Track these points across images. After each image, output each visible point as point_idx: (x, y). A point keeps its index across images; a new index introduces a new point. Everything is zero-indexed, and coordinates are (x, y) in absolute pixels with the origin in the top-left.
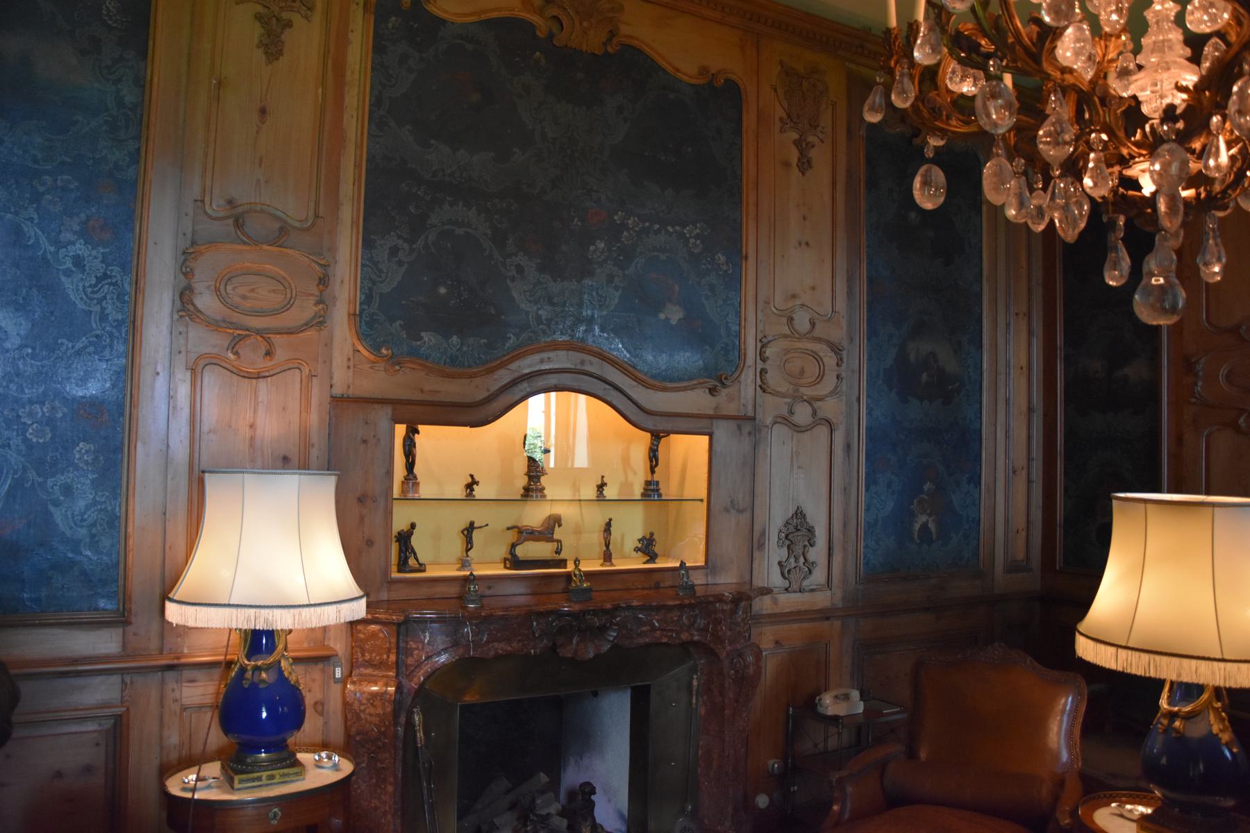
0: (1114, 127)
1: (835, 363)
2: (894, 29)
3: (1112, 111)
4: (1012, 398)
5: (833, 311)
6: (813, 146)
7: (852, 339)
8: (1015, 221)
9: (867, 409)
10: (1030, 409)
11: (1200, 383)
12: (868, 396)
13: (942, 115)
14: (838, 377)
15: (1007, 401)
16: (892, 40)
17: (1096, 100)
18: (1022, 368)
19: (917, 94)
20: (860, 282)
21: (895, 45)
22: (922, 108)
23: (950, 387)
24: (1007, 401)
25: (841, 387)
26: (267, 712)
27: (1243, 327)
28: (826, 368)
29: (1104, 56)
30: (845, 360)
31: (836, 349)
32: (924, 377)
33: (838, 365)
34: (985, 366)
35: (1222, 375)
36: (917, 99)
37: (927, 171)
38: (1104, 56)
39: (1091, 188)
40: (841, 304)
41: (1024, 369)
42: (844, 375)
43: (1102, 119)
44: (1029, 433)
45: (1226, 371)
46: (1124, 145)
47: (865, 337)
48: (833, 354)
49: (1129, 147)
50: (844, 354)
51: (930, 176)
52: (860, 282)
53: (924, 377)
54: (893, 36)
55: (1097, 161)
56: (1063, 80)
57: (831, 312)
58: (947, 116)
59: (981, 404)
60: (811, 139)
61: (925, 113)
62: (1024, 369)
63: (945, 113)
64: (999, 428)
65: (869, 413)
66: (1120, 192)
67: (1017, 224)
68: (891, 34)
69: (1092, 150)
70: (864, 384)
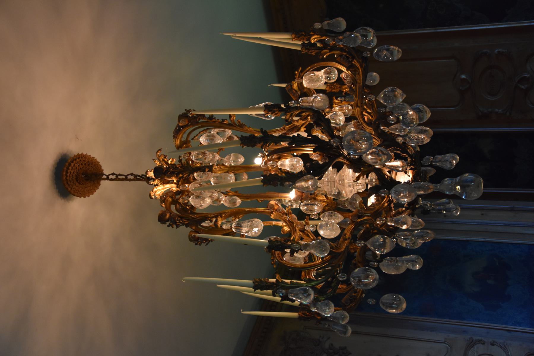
0: (373, 211)
1: (482, 345)
2: (299, 315)
3: (366, 212)
4: (504, 222)
5: (444, 343)
6: (332, 345)
7: (464, 331)
8: (422, 265)
9: (516, 326)
10: (512, 210)
11: (497, 110)
12: (506, 324)
13: (355, 296)
14: (493, 345)
15: (506, 225)
16: (306, 316)
17: (359, 220)
18: (482, 214)
19: (341, 308)
20: (423, 321)
21: (309, 315)
22: (349, 307)
23: (497, 264)
24: (506, 225)
25: (500, 343)
26: (460, 213)
27: (461, 88)
28: (486, 353)
29: (324, 202)
30: (480, 338)
31: (471, 344)
32: (490, 282)
33: (484, 344)
34: (481, 239)
35: (492, 98)
36: (344, 309)
37: (383, 305)
38: (324, 202)
39: (407, 226)
40: (440, 337)
41: (483, 213)
42: (491, 340)
43: (370, 218)
44: (528, 211)
45: (489, 96)
46: (383, 205)
47: (461, 321)
48: (476, 347)
49: (384, 203)
50: (475, 338)
51: (387, 303)
52: (423, 321)
53: (490, 282)
54: (303, 316)
55: (392, 221)
56: (349, 238)
57: (444, 344)
58: (355, 293)
59: (509, 243)
60: (327, 346)
61: (352, 305)
62: (483, 213)
63: (353, 294)
64: (526, 232)
65: (520, 324)
66: (407, 206)
67: (424, 263)
68: (302, 317)
69: (386, 223)
70: (497, 326)
